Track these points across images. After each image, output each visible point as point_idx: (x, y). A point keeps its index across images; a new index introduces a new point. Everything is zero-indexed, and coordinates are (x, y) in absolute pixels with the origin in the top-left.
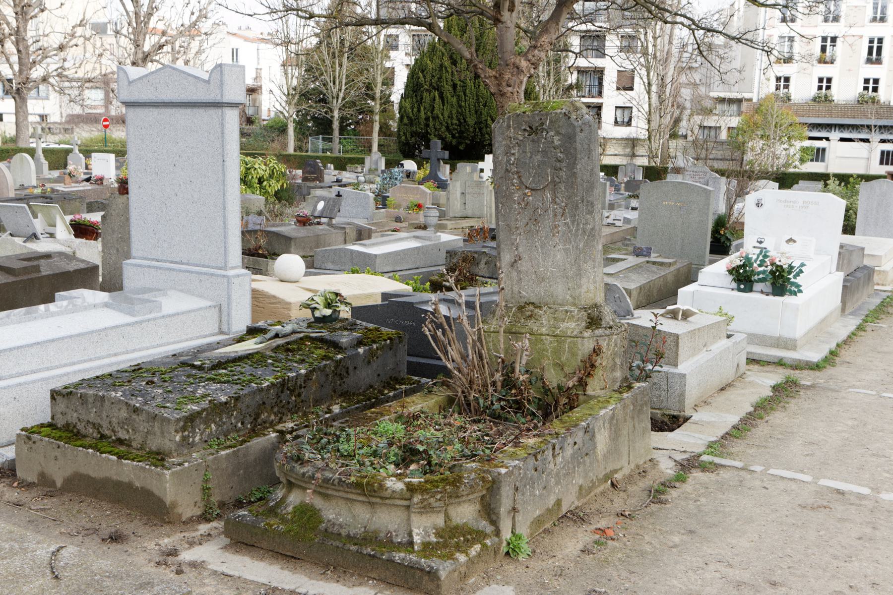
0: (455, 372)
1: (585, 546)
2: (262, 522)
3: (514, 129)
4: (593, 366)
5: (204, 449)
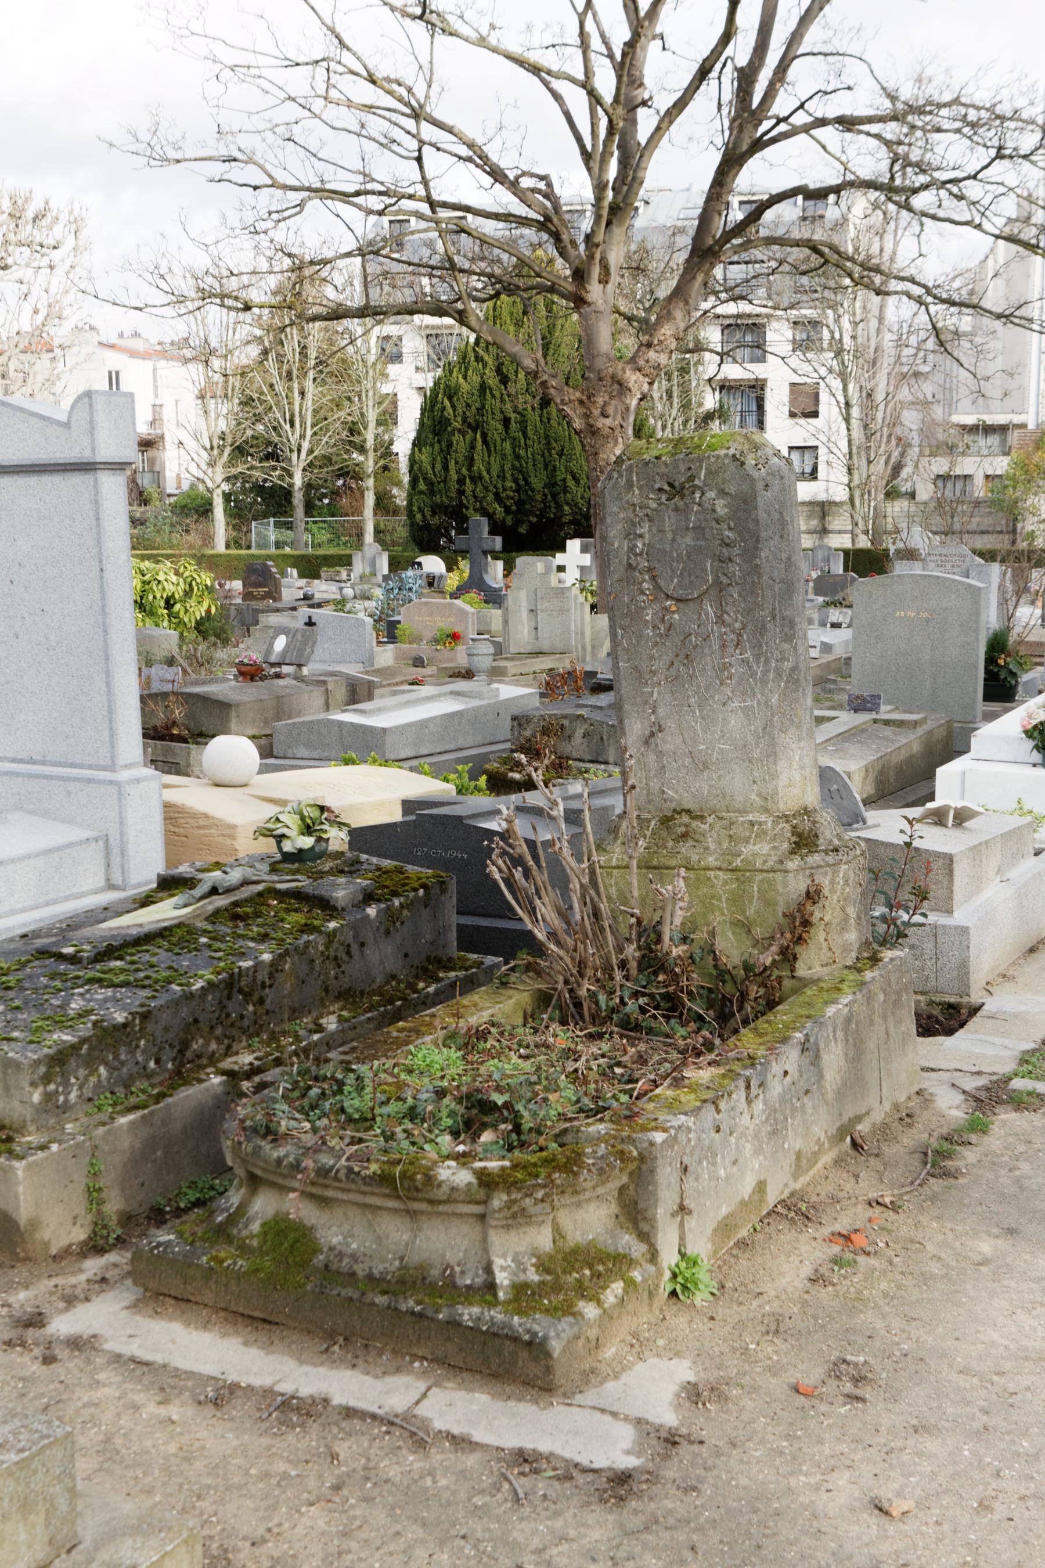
0: (552, 946)
1: (816, 1271)
2: (204, 1254)
3: (640, 488)
4: (806, 923)
5: (87, 1114)
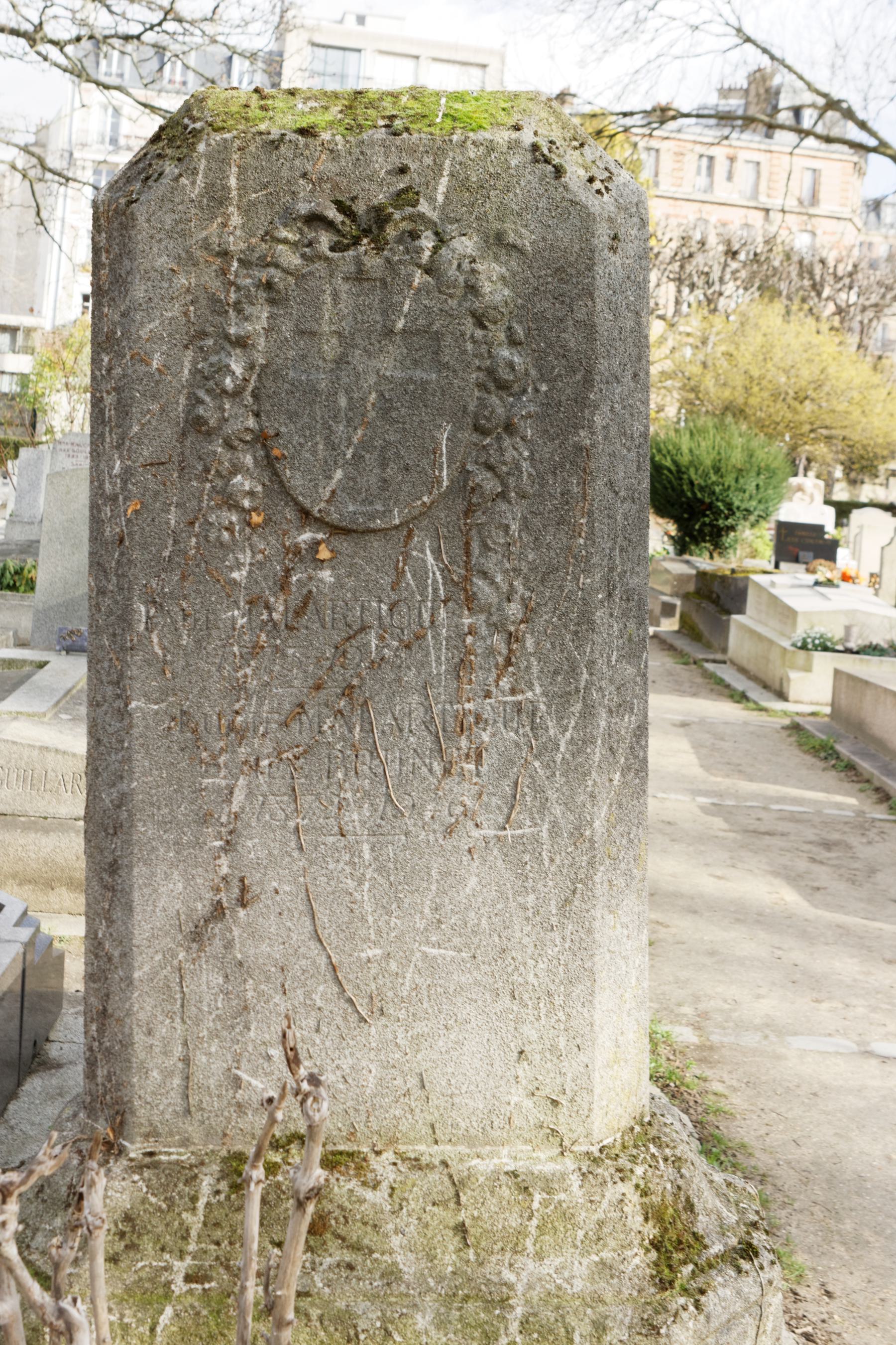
3: (247, 210)
